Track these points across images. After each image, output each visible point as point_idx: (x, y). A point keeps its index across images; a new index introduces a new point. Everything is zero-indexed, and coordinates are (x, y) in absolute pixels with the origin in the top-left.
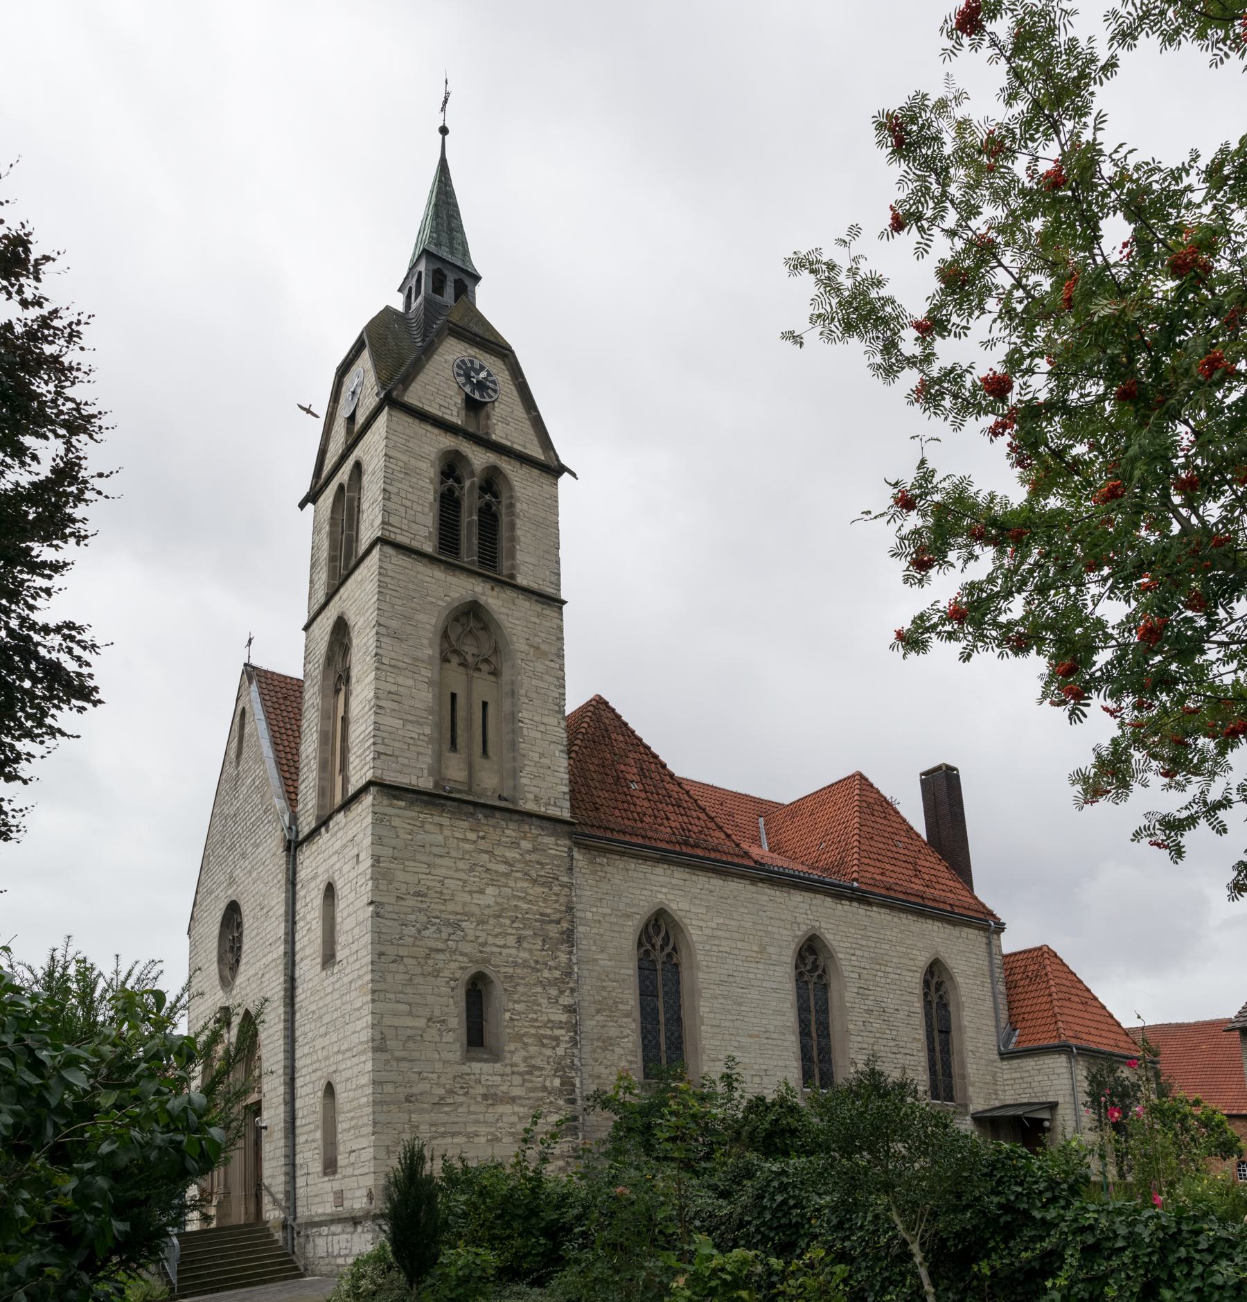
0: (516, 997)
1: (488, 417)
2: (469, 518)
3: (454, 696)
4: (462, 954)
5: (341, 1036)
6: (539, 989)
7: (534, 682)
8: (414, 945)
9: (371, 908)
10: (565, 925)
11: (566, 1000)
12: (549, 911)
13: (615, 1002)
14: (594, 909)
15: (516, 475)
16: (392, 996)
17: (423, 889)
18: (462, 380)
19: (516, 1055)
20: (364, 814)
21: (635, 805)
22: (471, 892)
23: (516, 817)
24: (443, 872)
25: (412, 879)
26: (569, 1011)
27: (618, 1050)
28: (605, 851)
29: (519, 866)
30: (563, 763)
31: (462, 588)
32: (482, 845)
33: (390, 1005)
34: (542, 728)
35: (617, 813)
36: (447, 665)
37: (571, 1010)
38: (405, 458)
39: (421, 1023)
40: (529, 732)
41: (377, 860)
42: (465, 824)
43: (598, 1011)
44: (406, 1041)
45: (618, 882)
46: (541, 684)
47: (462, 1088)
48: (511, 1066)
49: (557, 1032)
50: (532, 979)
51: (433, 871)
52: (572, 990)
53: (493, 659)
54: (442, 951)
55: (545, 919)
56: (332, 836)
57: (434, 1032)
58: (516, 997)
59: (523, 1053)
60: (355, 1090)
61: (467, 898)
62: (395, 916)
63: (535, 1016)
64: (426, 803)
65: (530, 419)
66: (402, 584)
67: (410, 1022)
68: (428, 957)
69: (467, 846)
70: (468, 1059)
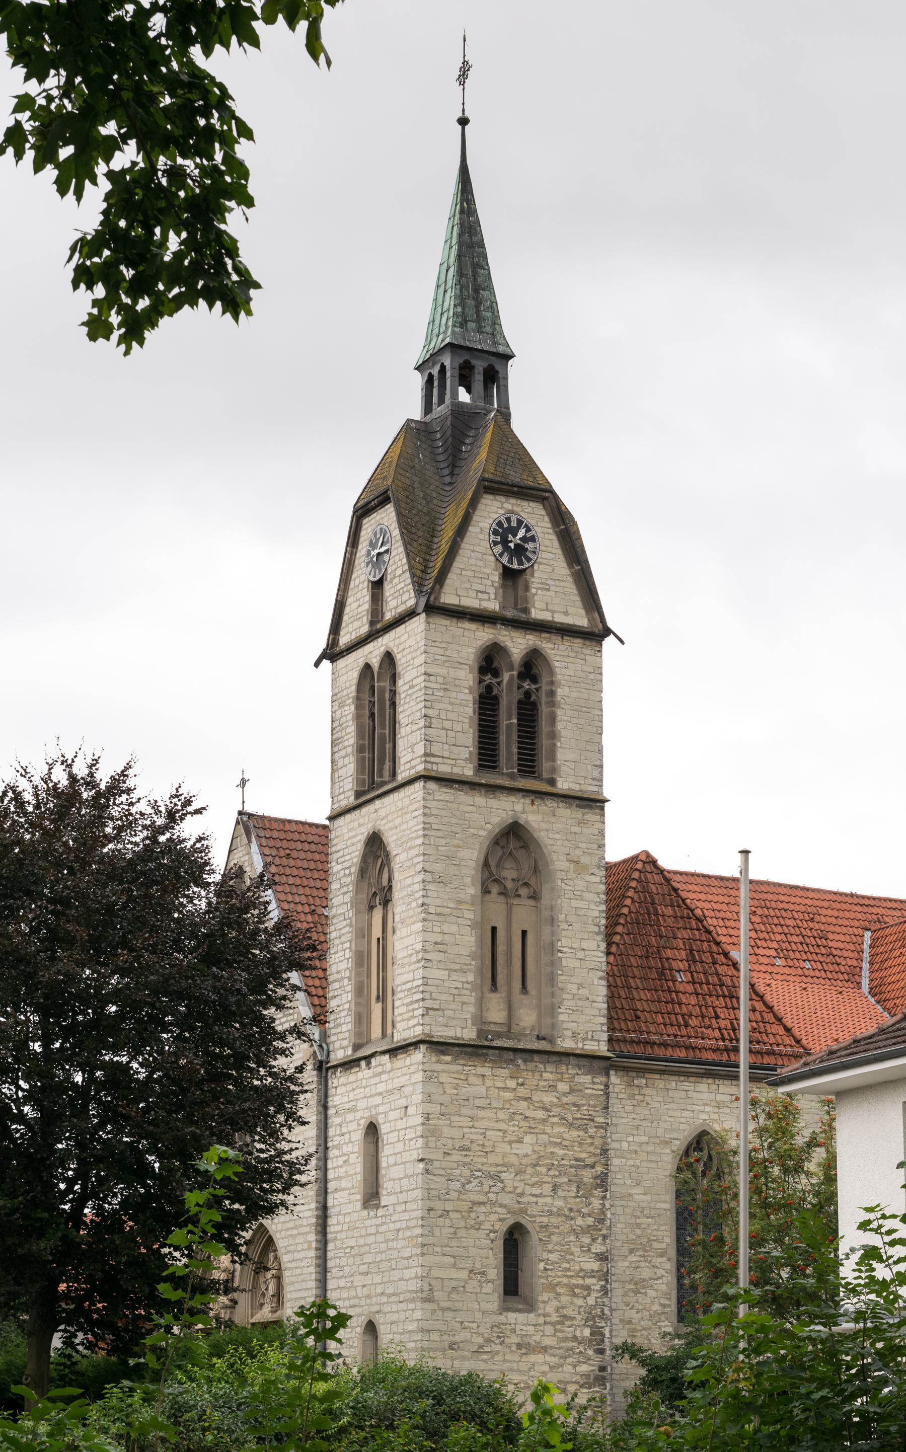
0: (550, 1246)
1: (527, 588)
2: (508, 721)
3: (494, 929)
4: (501, 1206)
5: (385, 1279)
6: (573, 1238)
7: (574, 903)
8: (459, 1199)
9: (421, 1165)
10: (599, 1169)
11: (598, 1248)
12: (584, 1155)
13: (649, 1240)
14: (631, 1139)
15: (556, 651)
16: (438, 1249)
17: (467, 1143)
18: (499, 549)
19: (548, 1303)
20: (413, 1068)
21: (680, 1004)
22: (510, 1143)
23: (554, 1058)
24: (484, 1124)
25: (456, 1133)
26: (601, 1259)
27: (652, 1293)
28: (642, 1071)
29: (556, 1110)
30: (602, 991)
31: (500, 810)
32: (522, 1092)
33: (437, 1258)
34: (581, 955)
35: (659, 1019)
36: (488, 897)
37: (602, 1258)
38: (443, 671)
39: (464, 1274)
40: (568, 961)
41: (427, 1117)
42: (505, 1072)
43: (631, 1251)
44: (450, 1293)
45: (657, 1105)
46: (581, 904)
47: (499, 1337)
48: (544, 1316)
49: (589, 1281)
50: (565, 1228)
51: (476, 1124)
52: (605, 1237)
53: (532, 882)
54: (483, 1203)
55: (581, 1165)
56: (375, 1075)
57: (474, 1283)
58: (550, 1246)
59: (555, 1303)
60: (401, 1334)
61: (507, 1148)
62: (442, 1172)
63: (567, 1265)
64: (471, 1055)
65: (572, 574)
66: (445, 820)
67: (454, 1274)
68: (470, 1210)
69: (508, 1095)
70: (506, 1309)
